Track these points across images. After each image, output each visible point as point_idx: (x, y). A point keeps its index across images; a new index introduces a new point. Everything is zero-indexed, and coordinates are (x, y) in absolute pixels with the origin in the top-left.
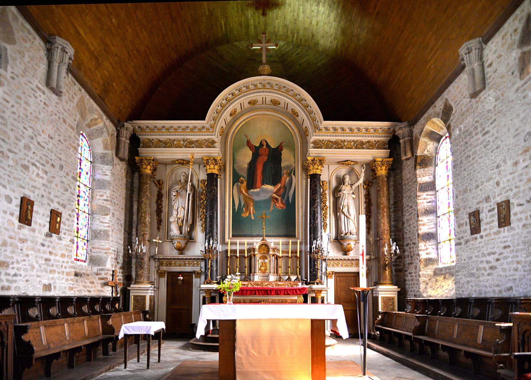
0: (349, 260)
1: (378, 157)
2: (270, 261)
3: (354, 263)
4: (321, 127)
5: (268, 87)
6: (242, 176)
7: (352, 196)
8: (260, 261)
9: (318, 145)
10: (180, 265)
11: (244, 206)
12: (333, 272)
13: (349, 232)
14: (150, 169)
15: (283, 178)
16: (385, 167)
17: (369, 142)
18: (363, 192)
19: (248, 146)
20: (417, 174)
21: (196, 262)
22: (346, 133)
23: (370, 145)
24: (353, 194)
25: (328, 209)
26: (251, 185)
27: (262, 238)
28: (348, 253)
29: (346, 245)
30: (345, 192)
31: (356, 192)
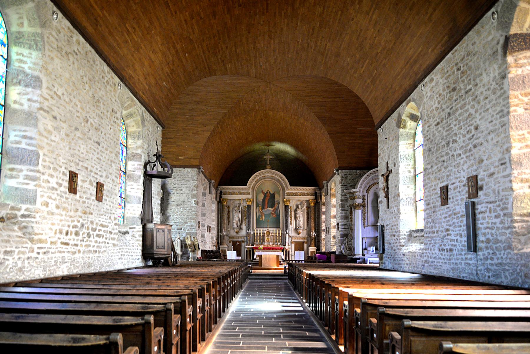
26: (263, 208)
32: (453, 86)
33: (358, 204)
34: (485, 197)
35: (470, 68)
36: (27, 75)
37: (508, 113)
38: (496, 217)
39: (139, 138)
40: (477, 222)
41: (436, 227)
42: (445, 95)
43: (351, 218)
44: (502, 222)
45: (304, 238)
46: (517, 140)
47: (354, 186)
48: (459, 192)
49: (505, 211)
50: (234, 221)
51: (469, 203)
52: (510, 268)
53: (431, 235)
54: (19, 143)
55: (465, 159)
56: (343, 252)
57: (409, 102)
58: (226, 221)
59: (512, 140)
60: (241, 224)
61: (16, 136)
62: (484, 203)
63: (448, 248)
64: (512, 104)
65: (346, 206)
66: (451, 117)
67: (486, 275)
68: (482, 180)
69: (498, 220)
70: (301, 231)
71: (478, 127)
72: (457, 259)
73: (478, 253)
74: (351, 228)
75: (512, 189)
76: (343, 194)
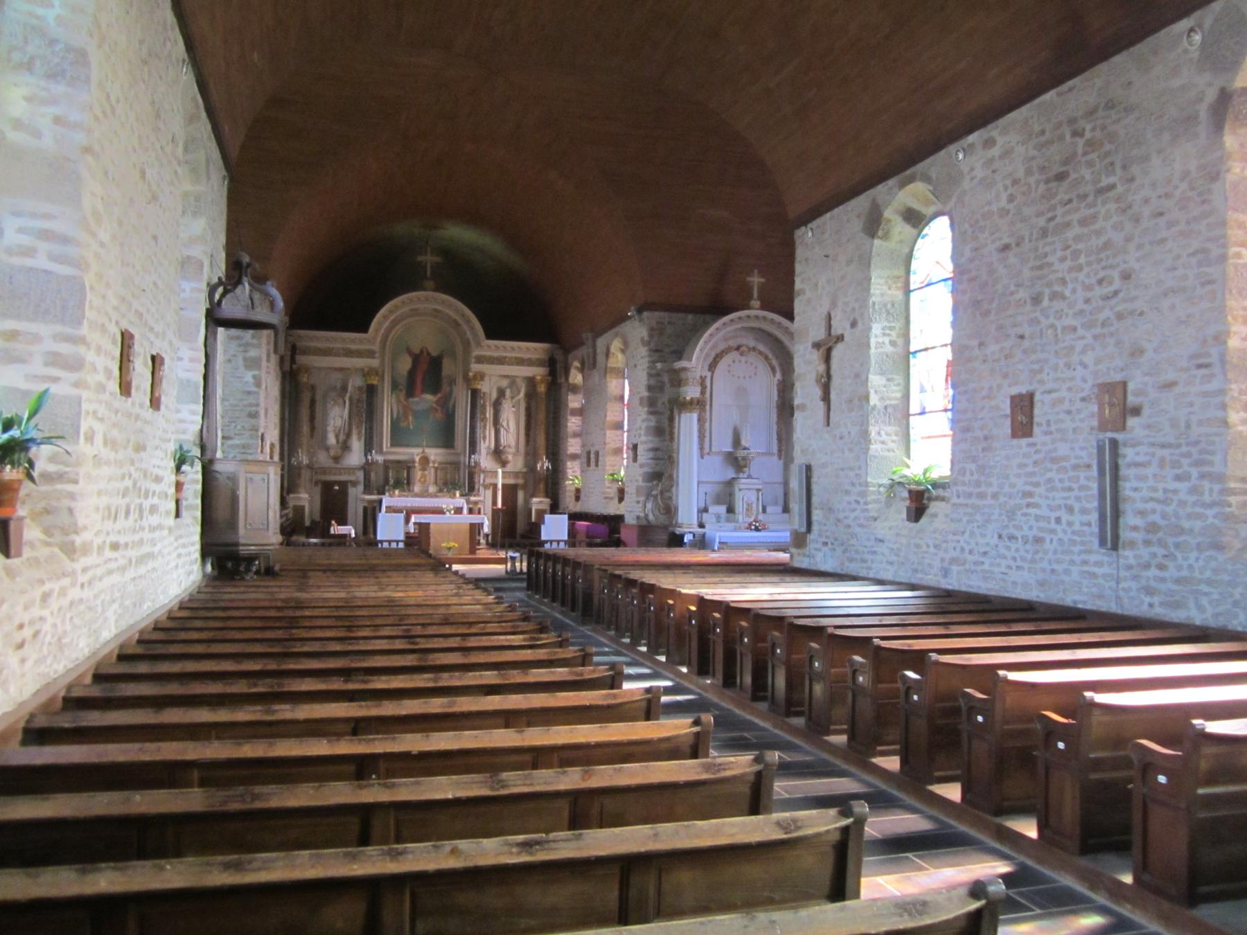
2: (430, 473)
9: (480, 360)
26: (410, 393)
32: (1057, 169)
33: (692, 398)
34: (1146, 432)
35: (1112, 137)
36: (53, 42)
37: (1223, 258)
38: (1178, 478)
39: (196, 212)
40: (1121, 483)
41: (990, 485)
42: (1034, 186)
43: (672, 433)
44: (1194, 490)
45: (516, 474)
46: (1240, 320)
47: (679, 354)
48: (1069, 412)
49: (1206, 469)
50: (330, 429)
51: (1103, 441)
52: (1212, 590)
53: (973, 500)
54: (29, 252)
55: (1089, 340)
56: (651, 517)
57: (911, 180)
58: (305, 429)
59: (1229, 318)
60: (349, 435)
61: (21, 230)
62: (1143, 444)
63: (1031, 534)
64: (1233, 239)
65: (660, 402)
66: (1049, 239)
67: (1143, 602)
68: (1139, 393)
69: (1183, 486)
70: (510, 457)
71: (1133, 276)
72: (1058, 562)
73: (1121, 551)
74: (670, 457)
75: (1225, 423)
76: (654, 372)
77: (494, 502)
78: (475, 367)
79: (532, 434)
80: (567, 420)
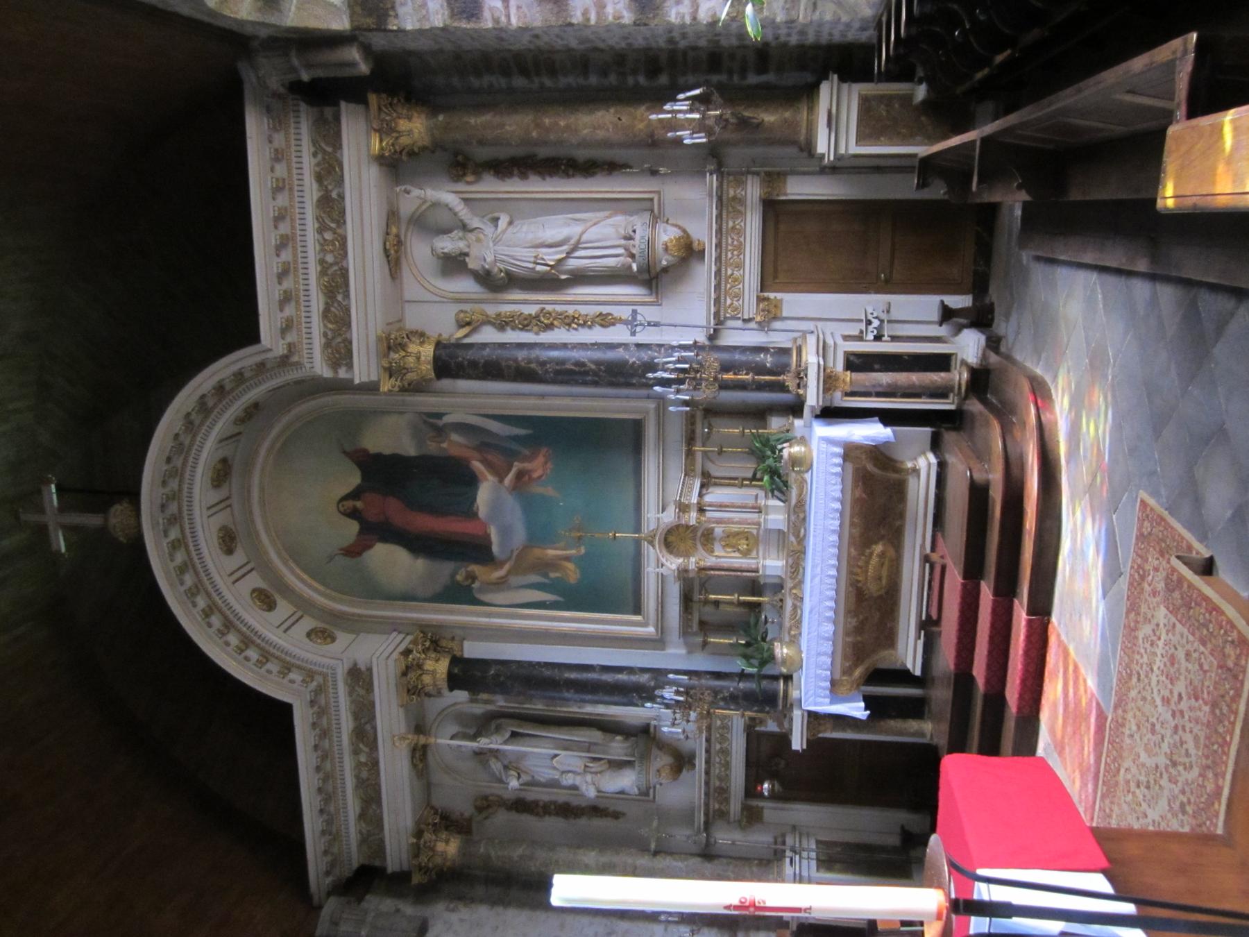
0: (719, 245)
1: (369, 150)
2: (719, 521)
3: (731, 224)
4: (280, 350)
5: (173, 508)
6: (453, 576)
7: (504, 231)
8: (719, 551)
9: (340, 353)
10: (727, 765)
11: (546, 575)
12: (760, 299)
13: (623, 242)
14: (447, 842)
15: (455, 452)
16: (401, 122)
17: (319, 178)
18: (490, 186)
19: (359, 554)
20: (417, 26)
21: (719, 723)
22: (295, 262)
23: (329, 173)
24: (495, 220)
25: (549, 308)
26: (478, 551)
27: (645, 544)
28: (695, 246)
29: (670, 258)
30: (490, 258)
31: (490, 209)
45: (727, 206)
77: (739, 841)
78: (363, 368)
79: (582, 155)
80: (500, 32)
